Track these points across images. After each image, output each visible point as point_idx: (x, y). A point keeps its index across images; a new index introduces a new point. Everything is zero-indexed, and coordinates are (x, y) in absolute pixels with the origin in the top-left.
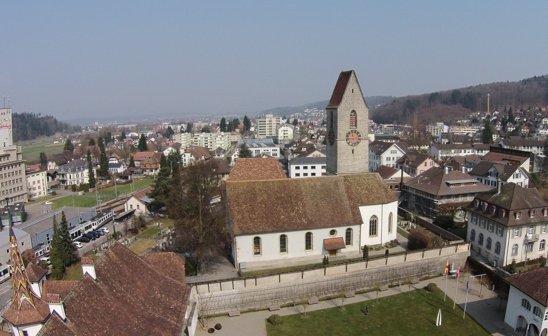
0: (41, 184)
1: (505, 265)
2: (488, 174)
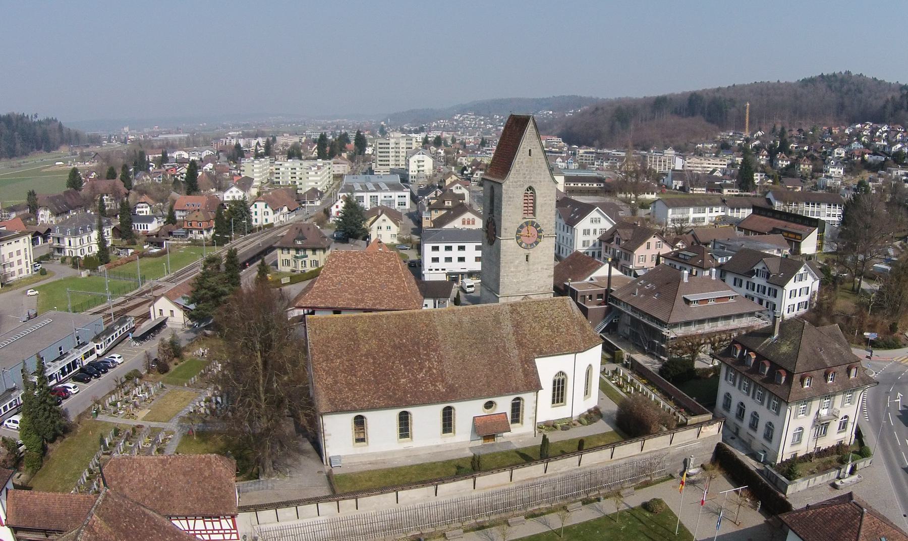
0: (22, 257)
1: (779, 461)
2: (751, 273)
